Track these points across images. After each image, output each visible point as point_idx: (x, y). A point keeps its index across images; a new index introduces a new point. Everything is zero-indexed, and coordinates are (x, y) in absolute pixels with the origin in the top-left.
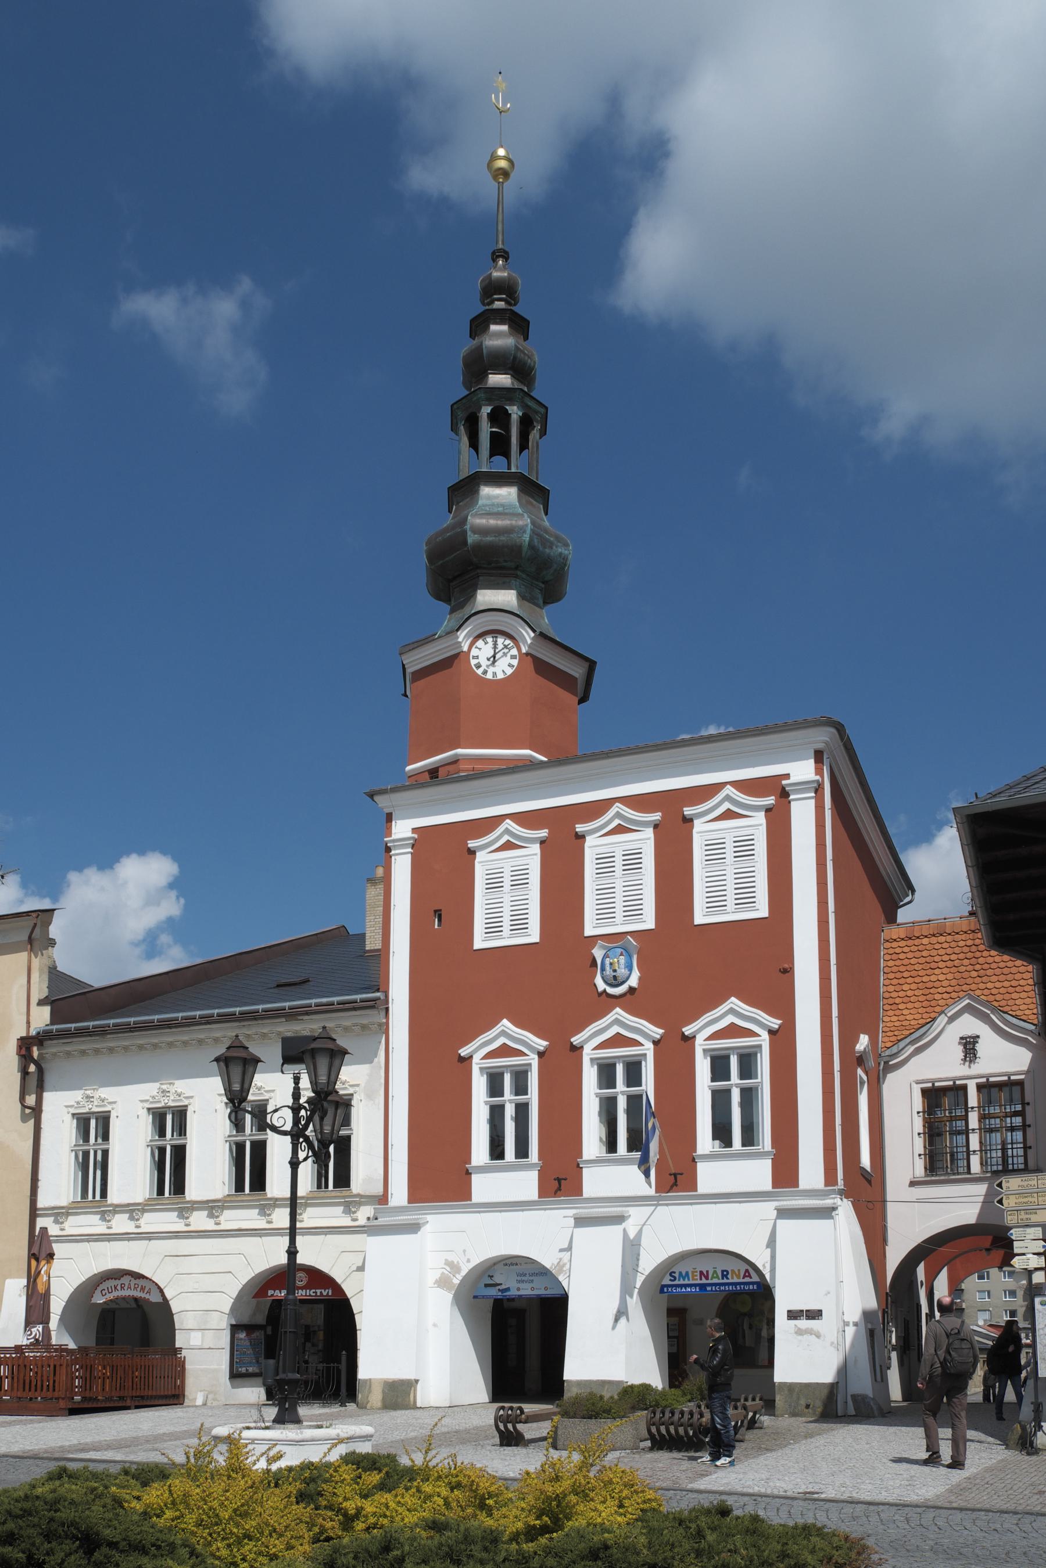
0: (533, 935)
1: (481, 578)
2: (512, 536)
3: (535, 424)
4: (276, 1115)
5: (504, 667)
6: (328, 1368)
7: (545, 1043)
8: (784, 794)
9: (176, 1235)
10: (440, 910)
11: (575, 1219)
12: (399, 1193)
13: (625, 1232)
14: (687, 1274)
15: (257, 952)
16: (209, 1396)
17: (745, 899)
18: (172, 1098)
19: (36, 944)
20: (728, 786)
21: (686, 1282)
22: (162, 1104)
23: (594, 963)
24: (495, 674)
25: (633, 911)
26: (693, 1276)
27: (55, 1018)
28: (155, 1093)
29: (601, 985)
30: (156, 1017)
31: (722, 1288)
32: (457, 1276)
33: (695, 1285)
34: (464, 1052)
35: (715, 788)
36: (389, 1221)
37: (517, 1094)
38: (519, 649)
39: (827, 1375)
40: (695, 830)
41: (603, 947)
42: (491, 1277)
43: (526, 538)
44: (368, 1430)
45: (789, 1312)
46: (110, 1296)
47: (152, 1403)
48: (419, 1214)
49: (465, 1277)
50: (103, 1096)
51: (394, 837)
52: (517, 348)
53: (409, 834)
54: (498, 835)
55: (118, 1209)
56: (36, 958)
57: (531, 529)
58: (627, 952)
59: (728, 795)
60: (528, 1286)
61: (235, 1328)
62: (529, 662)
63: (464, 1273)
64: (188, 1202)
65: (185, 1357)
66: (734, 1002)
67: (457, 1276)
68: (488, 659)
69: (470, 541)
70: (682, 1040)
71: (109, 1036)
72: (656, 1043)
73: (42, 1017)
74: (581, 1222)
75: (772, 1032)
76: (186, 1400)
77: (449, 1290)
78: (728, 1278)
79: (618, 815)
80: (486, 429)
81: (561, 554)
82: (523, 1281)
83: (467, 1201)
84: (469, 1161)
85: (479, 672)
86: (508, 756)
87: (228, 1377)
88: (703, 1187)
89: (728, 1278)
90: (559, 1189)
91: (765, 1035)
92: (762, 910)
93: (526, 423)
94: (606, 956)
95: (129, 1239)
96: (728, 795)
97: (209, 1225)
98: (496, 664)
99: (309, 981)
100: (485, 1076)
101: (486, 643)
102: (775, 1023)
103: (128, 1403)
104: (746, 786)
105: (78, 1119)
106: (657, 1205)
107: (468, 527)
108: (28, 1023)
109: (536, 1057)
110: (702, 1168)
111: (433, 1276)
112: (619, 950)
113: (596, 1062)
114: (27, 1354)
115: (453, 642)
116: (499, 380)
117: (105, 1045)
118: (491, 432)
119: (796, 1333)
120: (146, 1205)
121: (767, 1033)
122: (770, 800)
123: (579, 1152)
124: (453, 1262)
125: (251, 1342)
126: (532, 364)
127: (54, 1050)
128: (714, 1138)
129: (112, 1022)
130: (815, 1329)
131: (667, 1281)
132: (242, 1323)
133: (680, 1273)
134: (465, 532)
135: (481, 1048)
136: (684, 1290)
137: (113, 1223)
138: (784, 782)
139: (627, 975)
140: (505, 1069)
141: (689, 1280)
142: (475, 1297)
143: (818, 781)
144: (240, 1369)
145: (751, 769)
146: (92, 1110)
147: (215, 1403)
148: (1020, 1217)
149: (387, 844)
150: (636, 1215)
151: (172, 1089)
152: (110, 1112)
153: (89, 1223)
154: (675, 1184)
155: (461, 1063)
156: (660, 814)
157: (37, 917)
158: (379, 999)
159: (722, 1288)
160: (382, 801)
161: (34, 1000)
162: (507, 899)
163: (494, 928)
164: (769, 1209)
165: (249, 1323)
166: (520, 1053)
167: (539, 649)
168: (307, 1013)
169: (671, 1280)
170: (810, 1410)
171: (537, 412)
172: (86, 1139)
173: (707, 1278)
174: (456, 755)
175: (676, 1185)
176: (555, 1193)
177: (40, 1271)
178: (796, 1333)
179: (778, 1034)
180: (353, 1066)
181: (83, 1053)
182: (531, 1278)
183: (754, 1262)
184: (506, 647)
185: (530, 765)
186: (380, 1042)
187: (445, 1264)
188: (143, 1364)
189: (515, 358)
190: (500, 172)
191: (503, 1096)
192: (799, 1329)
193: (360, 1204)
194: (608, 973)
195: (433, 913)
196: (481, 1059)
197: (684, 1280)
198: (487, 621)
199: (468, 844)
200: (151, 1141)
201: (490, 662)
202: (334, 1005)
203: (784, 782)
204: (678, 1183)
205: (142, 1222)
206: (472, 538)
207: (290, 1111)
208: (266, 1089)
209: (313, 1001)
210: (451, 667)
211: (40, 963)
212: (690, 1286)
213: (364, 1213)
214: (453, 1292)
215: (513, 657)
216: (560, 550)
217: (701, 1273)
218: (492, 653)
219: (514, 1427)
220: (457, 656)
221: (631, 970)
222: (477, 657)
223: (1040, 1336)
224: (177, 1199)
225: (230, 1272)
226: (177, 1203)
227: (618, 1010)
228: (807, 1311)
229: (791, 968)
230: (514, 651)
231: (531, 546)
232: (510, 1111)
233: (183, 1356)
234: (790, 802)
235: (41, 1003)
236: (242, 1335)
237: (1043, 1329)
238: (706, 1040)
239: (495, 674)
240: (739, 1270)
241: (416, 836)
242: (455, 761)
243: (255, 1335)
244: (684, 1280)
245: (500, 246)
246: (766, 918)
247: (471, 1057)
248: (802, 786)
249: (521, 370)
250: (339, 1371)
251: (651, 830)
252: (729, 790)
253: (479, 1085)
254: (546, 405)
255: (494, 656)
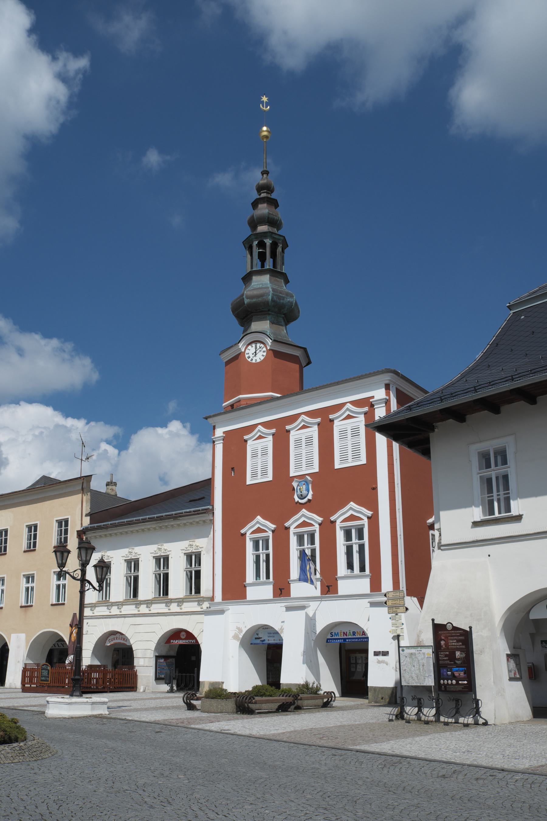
0: (270, 477)
1: (254, 317)
2: (264, 298)
3: (279, 244)
4: (75, 573)
5: (260, 357)
6: (182, 676)
7: (371, 513)
8: (372, 406)
9: (134, 616)
10: (234, 468)
11: (286, 607)
12: (218, 597)
13: (307, 614)
14: (338, 633)
15: (201, 483)
16: (146, 688)
17: (356, 456)
18: (133, 555)
19: (85, 490)
20: (348, 404)
21: (338, 637)
22: (190, 551)
23: (294, 489)
24: (256, 360)
25: (310, 464)
26: (341, 634)
27: (92, 522)
28: (187, 546)
29: (297, 499)
30: (126, 520)
31: (353, 640)
32: (241, 634)
33: (341, 639)
34: (243, 531)
35: (342, 405)
36: (214, 609)
37: (347, 541)
38: (266, 348)
39: (390, 684)
40: (334, 425)
41: (297, 481)
42: (257, 634)
43: (270, 297)
44: (106, 700)
45: (374, 652)
46: (112, 643)
47: (127, 690)
48: (224, 606)
49: (244, 635)
50: (108, 555)
51: (216, 436)
52: (269, 213)
53: (222, 435)
54: (255, 433)
55: (172, 601)
56: (85, 496)
57: (272, 294)
58: (307, 483)
59: (347, 408)
60: (272, 639)
61: (157, 658)
62: (271, 352)
63: (244, 633)
64: (139, 601)
65: (136, 670)
66: (352, 504)
67: (241, 634)
68: (253, 354)
69: (246, 302)
70: (331, 523)
71: (109, 529)
72: (320, 525)
73: (87, 521)
74: (288, 609)
75: (369, 518)
76: (138, 689)
77: (238, 640)
78: (355, 636)
79: (303, 421)
80: (256, 251)
81: (289, 301)
82: (270, 637)
83: (244, 599)
84: (245, 581)
85: (249, 360)
86: (262, 396)
87: (154, 679)
88: (249, 597)
89: (355, 636)
90: (281, 594)
91: (366, 520)
92: (363, 461)
93: (274, 246)
94: (298, 485)
95: (117, 617)
96: (347, 408)
97: (178, 609)
98: (256, 356)
99: (204, 498)
100: (343, 531)
101: (252, 347)
102: (370, 513)
103: (106, 690)
104: (355, 403)
105: (156, 559)
106: (321, 601)
107: (244, 296)
108: (82, 524)
109: (271, 533)
110: (340, 583)
111: (232, 634)
112: (303, 482)
113: (296, 534)
114: (67, 668)
115: (238, 348)
116: (263, 228)
117: (108, 533)
118: (258, 252)
119: (377, 662)
120: (123, 602)
121: (366, 518)
122: (366, 409)
123: (289, 577)
124: (239, 627)
125: (167, 664)
126: (278, 218)
127: (90, 536)
128: (348, 569)
129: (110, 523)
130: (386, 660)
131: (329, 637)
132: (162, 655)
133: (335, 633)
134: (243, 299)
135: (295, 523)
136: (336, 641)
137: (112, 610)
138: (371, 400)
139: (306, 494)
140: (304, 533)
141: (339, 636)
142: (251, 644)
143: (386, 399)
144: (161, 676)
145: (381, 390)
146: (193, 551)
147: (149, 691)
148: (393, 610)
149: (372, 403)
150: (313, 605)
151: (133, 551)
152: (111, 562)
153: (102, 610)
154: (329, 591)
155: (332, 524)
156: (275, 429)
157: (83, 479)
158: (209, 509)
159: (353, 640)
160: (210, 421)
161: (84, 514)
162: (259, 461)
163: (254, 475)
164: (365, 602)
165: (166, 655)
166: (265, 531)
167: (276, 347)
168: (180, 517)
169: (331, 636)
170: (383, 700)
171: (279, 239)
172: (191, 565)
173: (346, 635)
174: (239, 398)
175: (329, 591)
176: (280, 595)
177: (73, 632)
178: (377, 662)
179: (371, 519)
180: (201, 539)
181: (101, 536)
182: (274, 635)
183: (191, 632)
184: (260, 348)
185: (273, 399)
186: (211, 528)
187: (236, 628)
188: (62, 671)
189: (268, 218)
190: (264, 137)
191: (352, 541)
192: (379, 660)
193: (204, 601)
194: (299, 493)
195: (231, 469)
196: (250, 534)
197: (337, 636)
198: (250, 338)
199: (244, 438)
200: (155, 571)
201: (254, 355)
202: (191, 512)
203: (371, 400)
204: (330, 590)
205: (122, 610)
206: (246, 301)
207: (80, 571)
208: (168, 550)
209: (184, 511)
210: (238, 359)
211: (86, 498)
212: (339, 639)
213: (206, 605)
214: (239, 642)
215: (264, 352)
216: (288, 300)
217: (344, 633)
218: (255, 351)
219: (190, 701)
220: (240, 354)
221: (308, 491)
222: (248, 353)
223: (402, 666)
224: (135, 599)
225: (154, 632)
226: (134, 602)
227: (304, 510)
228: (382, 652)
229: (376, 487)
230: (265, 349)
231: (273, 300)
232: (355, 548)
233: (135, 669)
234: (374, 409)
235: (86, 515)
236: (162, 660)
237: (403, 662)
238: (294, 528)
239: (256, 360)
240: (360, 632)
241: (224, 435)
242: (239, 401)
243: (170, 660)
244: (337, 636)
245: (265, 169)
246: (365, 464)
247: (246, 533)
248: (379, 401)
249: (274, 222)
250: (194, 677)
251: (363, 415)
252: (349, 406)
253: (249, 545)
254: (283, 235)
255: (255, 352)
